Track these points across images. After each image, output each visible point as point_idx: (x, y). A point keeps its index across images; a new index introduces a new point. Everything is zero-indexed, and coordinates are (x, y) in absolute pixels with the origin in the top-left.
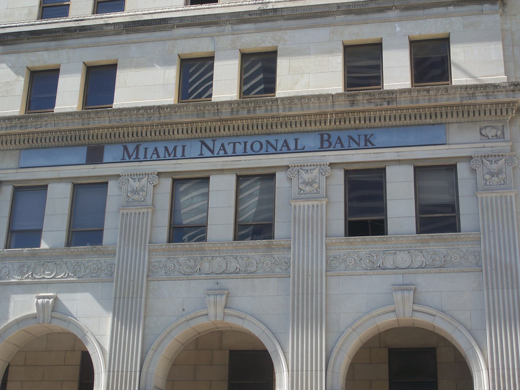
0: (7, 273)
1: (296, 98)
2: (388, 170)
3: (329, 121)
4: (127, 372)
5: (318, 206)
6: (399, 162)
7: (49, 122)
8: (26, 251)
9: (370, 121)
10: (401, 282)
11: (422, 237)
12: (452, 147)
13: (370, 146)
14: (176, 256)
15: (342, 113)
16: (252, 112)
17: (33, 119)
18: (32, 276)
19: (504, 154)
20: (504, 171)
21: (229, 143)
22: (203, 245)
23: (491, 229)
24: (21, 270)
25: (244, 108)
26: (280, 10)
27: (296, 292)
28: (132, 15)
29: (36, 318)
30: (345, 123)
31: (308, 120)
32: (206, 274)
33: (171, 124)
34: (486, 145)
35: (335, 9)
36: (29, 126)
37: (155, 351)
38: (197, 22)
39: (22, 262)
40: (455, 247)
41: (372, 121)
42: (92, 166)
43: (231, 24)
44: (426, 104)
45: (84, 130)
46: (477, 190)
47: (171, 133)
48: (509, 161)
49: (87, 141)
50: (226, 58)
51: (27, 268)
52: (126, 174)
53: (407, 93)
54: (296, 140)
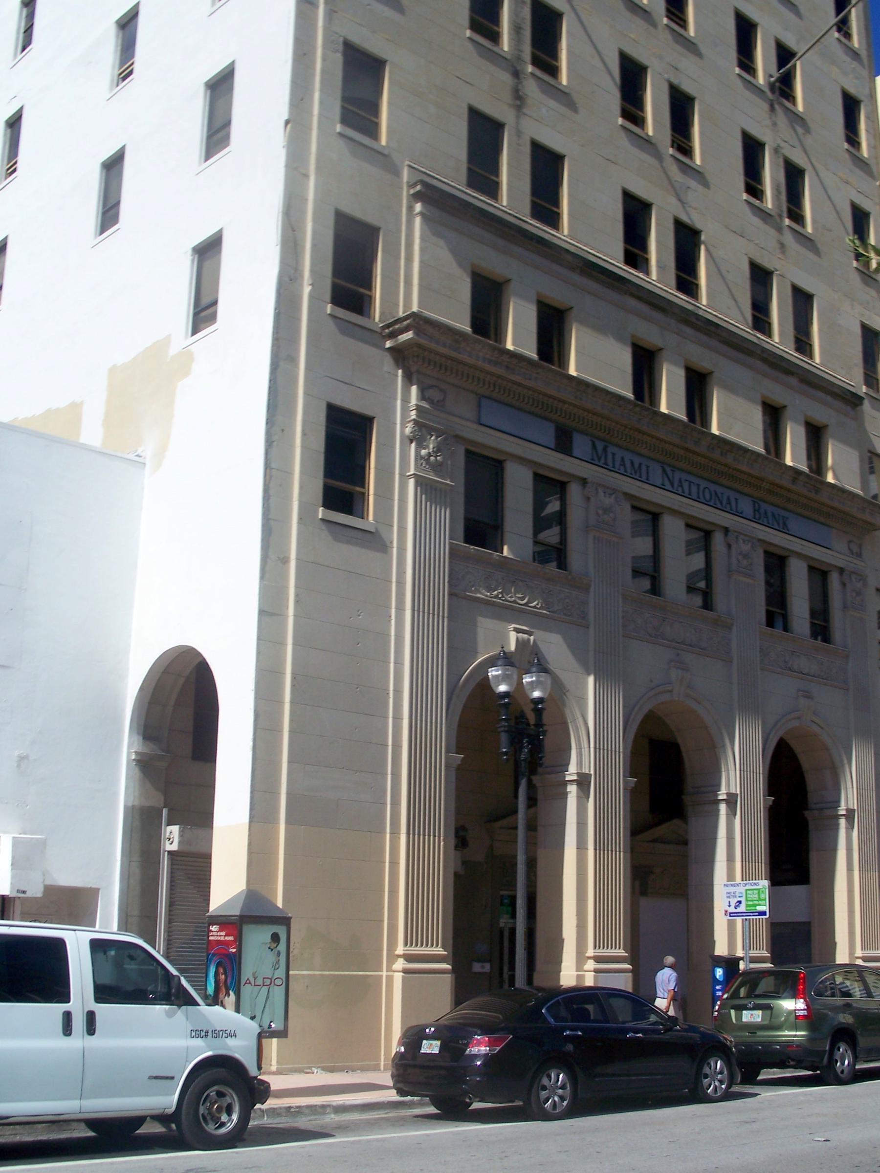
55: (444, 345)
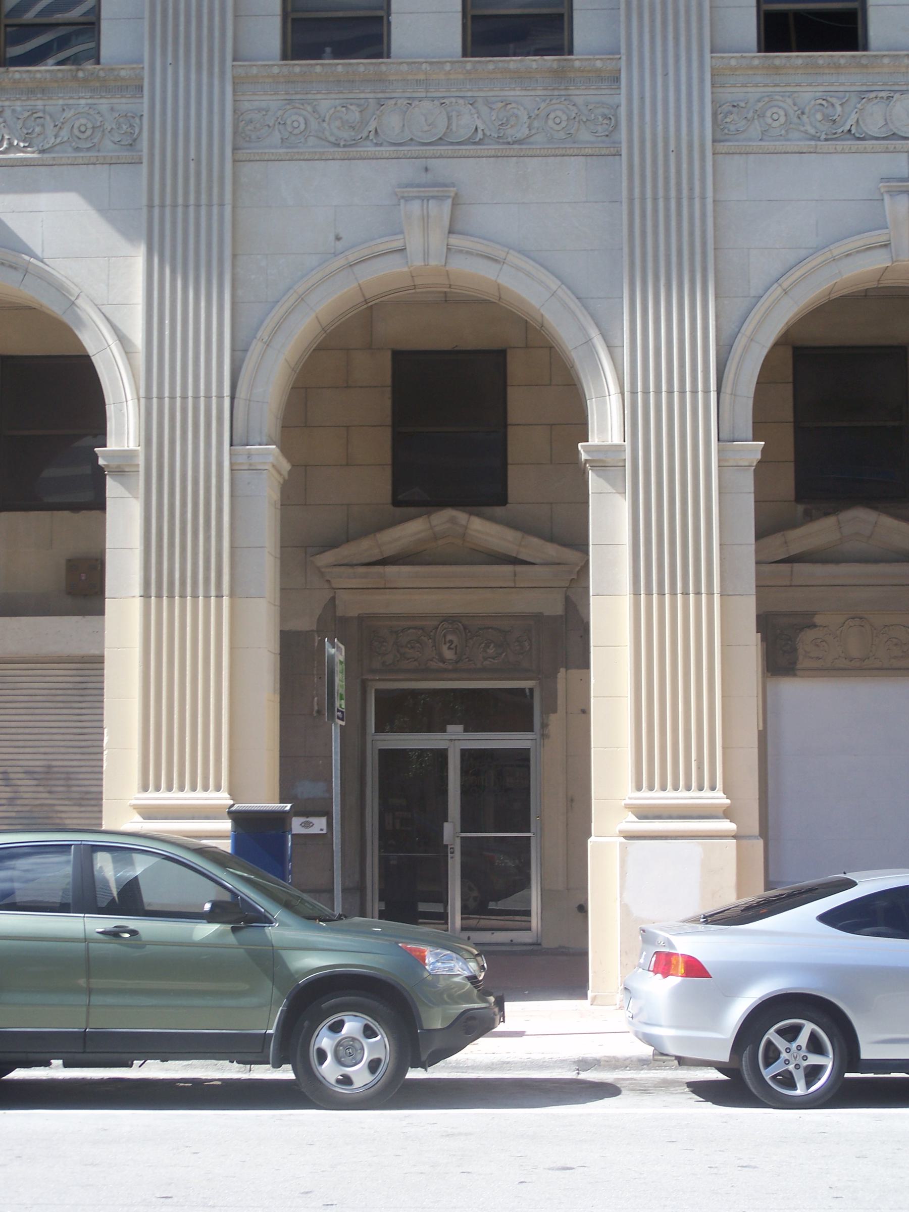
4: (196, 398)
14: (309, 96)
22: (384, 68)
23: (672, 146)
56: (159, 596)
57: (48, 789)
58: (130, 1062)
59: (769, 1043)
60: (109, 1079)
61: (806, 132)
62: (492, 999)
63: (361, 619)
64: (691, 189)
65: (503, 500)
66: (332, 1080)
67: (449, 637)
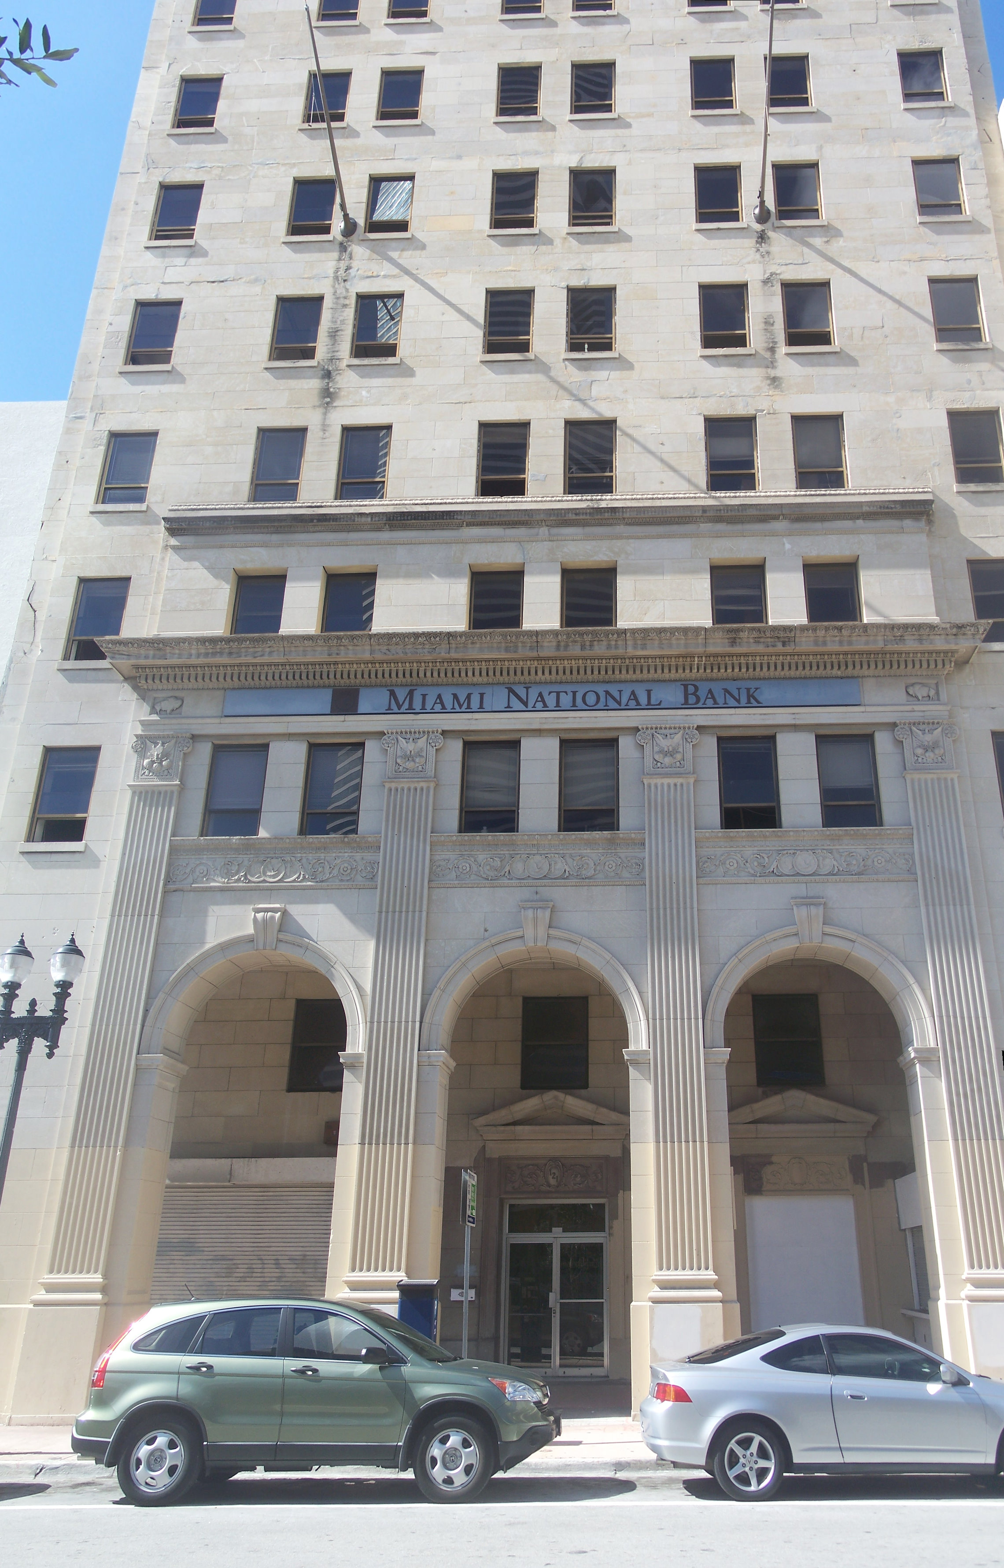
0: (205, 873)
1: (652, 631)
2: (779, 737)
3: (696, 666)
4: (400, 1022)
5: (682, 785)
6: (795, 728)
7: (276, 649)
8: (236, 839)
9: (754, 669)
10: (804, 894)
11: (832, 832)
12: (868, 709)
13: (755, 704)
14: (472, 853)
15: (716, 656)
16: (588, 647)
17: (250, 644)
18: (246, 878)
19: (940, 721)
20: (941, 744)
21: (550, 693)
22: (514, 838)
23: (674, 881)
24: (227, 869)
25: (576, 642)
26: (621, 510)
27: (655, 906)
28: (397, 505)
29: (253, 941)
30: (719, 670)
31: (666, 664)
32: (519, 879)
33: (464, 661)
34: (916, 708)
35: (700, 514)
36: (243, 654)
37: (443, 991)
38: (498, 519)
39: (229, 856)
40: (877, 847)
41: (758, 669)
42: (341, 718)
43: (547, 526)
44: (836, 648)
45: (328, 664)
46: (905, 769)
47: (463, 674)
48: (947, 732)
49: (332, 680)
50: (542, 572)
51: (237, 867)
52: (394, 731)
53: (810, 631)
54: (649, 692)
55: (146, 657)
56: (370, 1144)
57: (302, 1270)
58: (309, 1468)
59: (732, 1450)
60: (302, 1479)
61: (749, 872)
62: (552, 1418)
63: (500, 1159)
64: (685, 903)
65: (586, 1086)
66: (440, 1481)
67: (553, 1171)
